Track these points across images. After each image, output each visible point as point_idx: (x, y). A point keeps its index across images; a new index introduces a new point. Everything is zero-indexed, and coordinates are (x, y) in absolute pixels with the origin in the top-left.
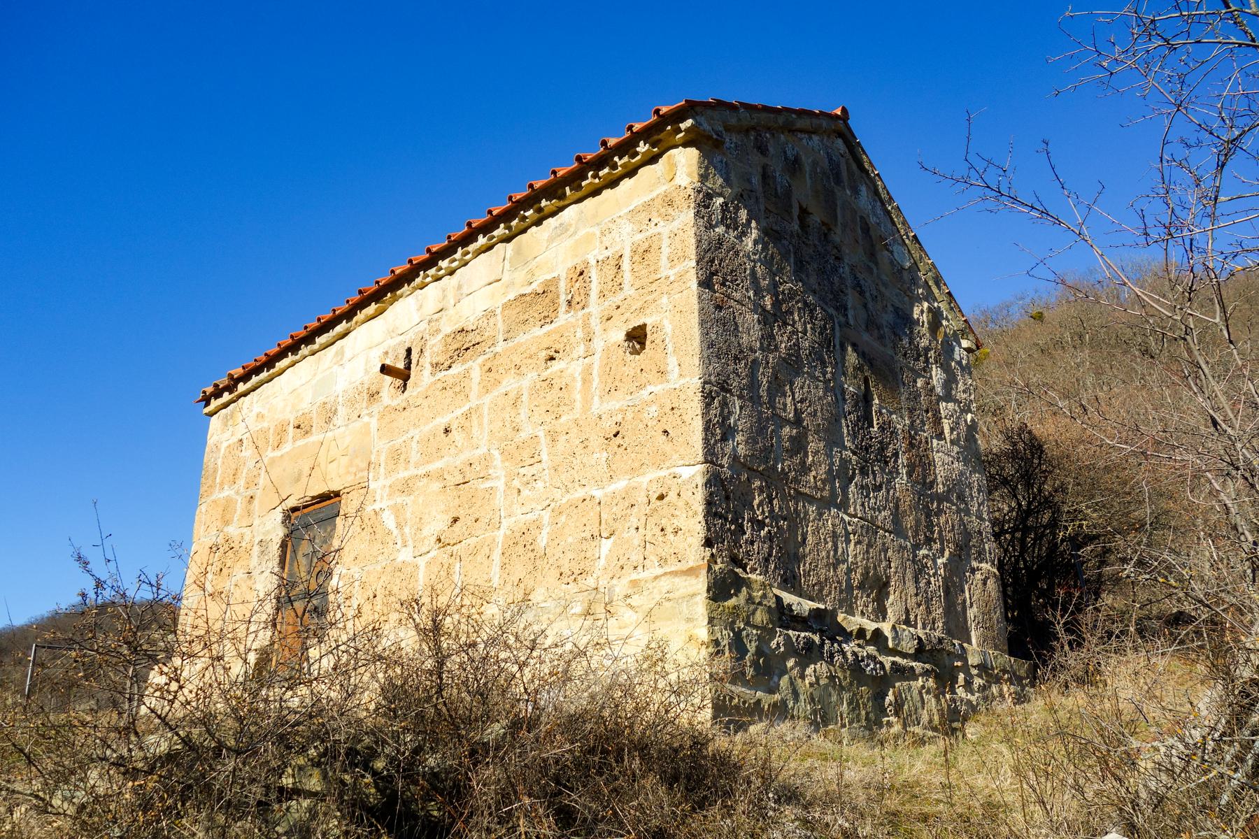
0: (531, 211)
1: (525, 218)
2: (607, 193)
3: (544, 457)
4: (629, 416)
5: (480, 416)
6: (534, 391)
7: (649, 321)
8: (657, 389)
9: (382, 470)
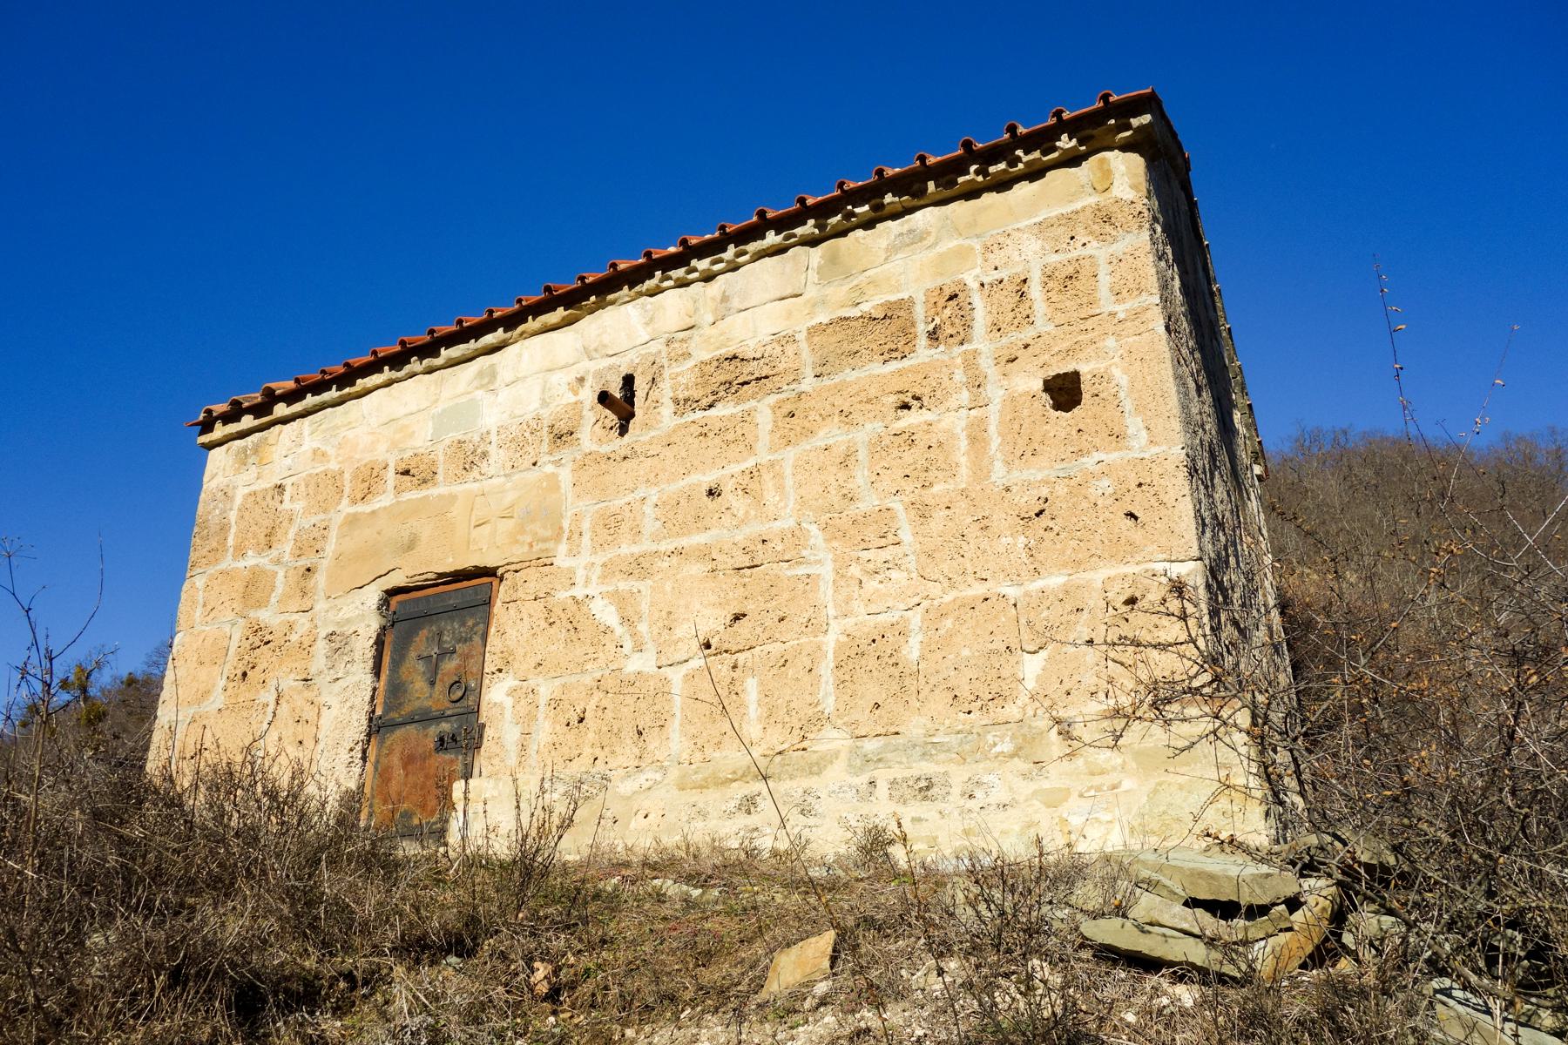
0: (866, 207)
1: (853, 214)
2: (989, 198)
3: (906, 535)
4: (1061, 490)
5: (778, 476)
6: (878, 447)
7: (1085, 369)
8: (1112, 457)
9: (586, 540)
